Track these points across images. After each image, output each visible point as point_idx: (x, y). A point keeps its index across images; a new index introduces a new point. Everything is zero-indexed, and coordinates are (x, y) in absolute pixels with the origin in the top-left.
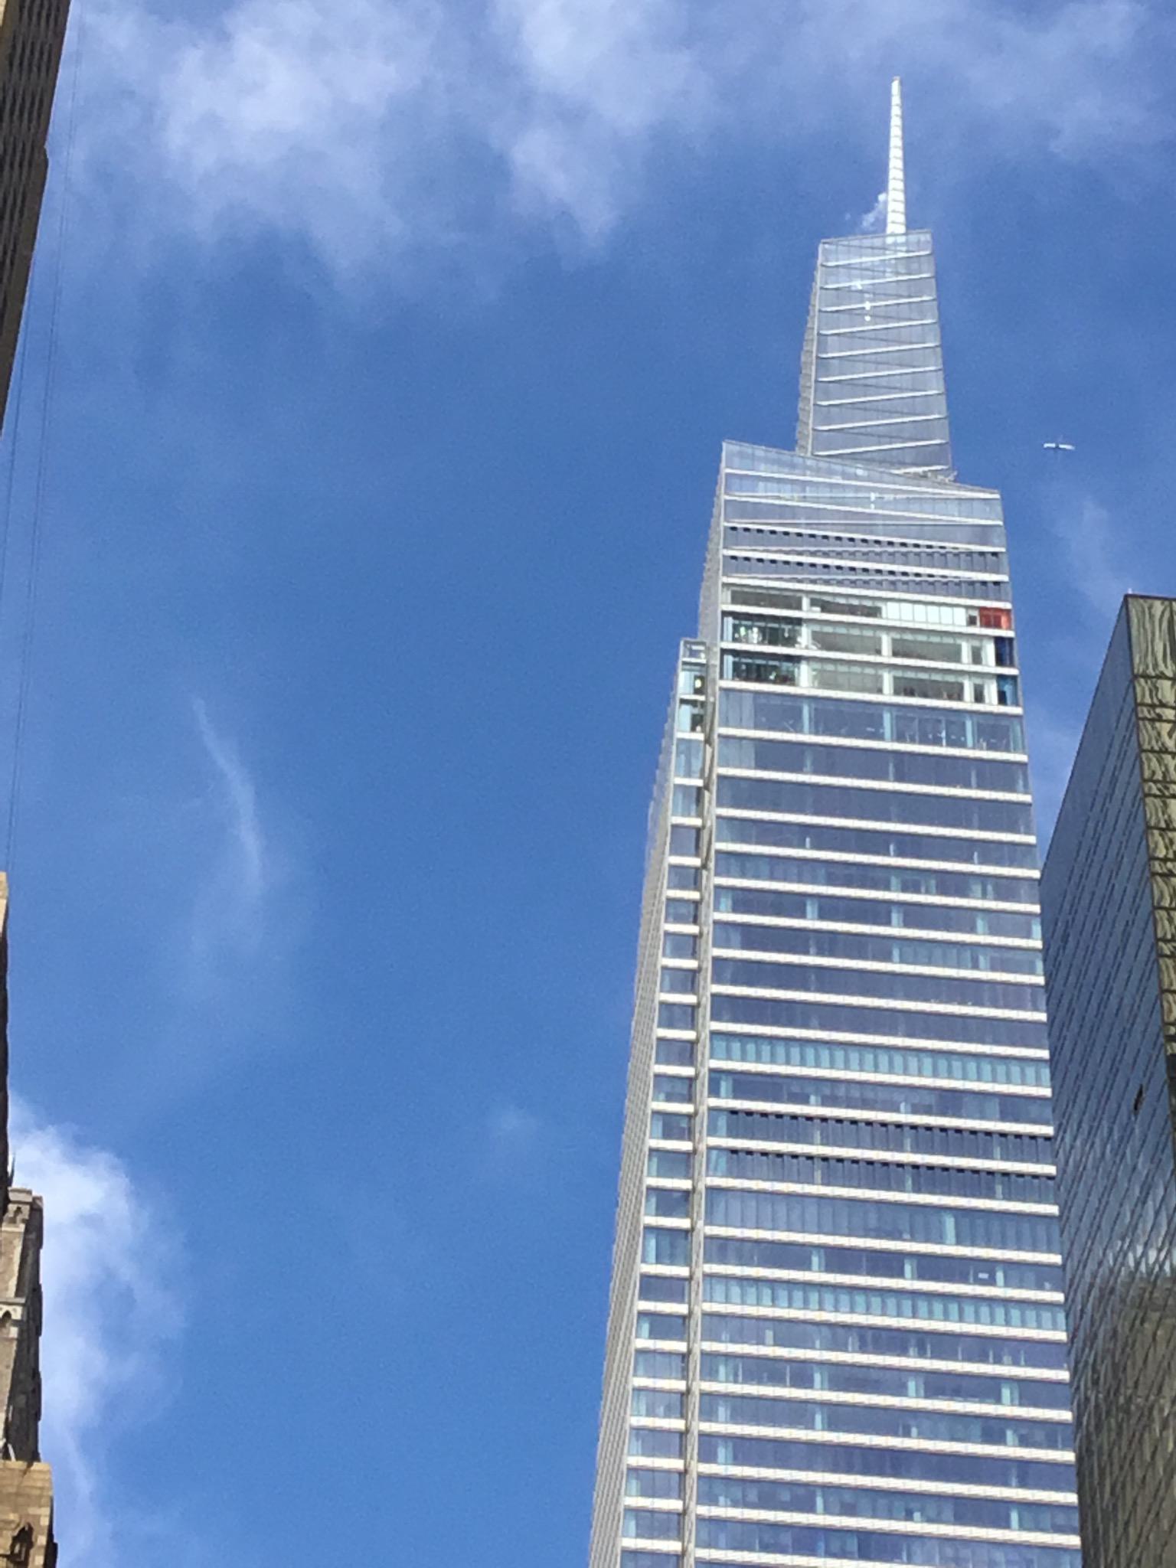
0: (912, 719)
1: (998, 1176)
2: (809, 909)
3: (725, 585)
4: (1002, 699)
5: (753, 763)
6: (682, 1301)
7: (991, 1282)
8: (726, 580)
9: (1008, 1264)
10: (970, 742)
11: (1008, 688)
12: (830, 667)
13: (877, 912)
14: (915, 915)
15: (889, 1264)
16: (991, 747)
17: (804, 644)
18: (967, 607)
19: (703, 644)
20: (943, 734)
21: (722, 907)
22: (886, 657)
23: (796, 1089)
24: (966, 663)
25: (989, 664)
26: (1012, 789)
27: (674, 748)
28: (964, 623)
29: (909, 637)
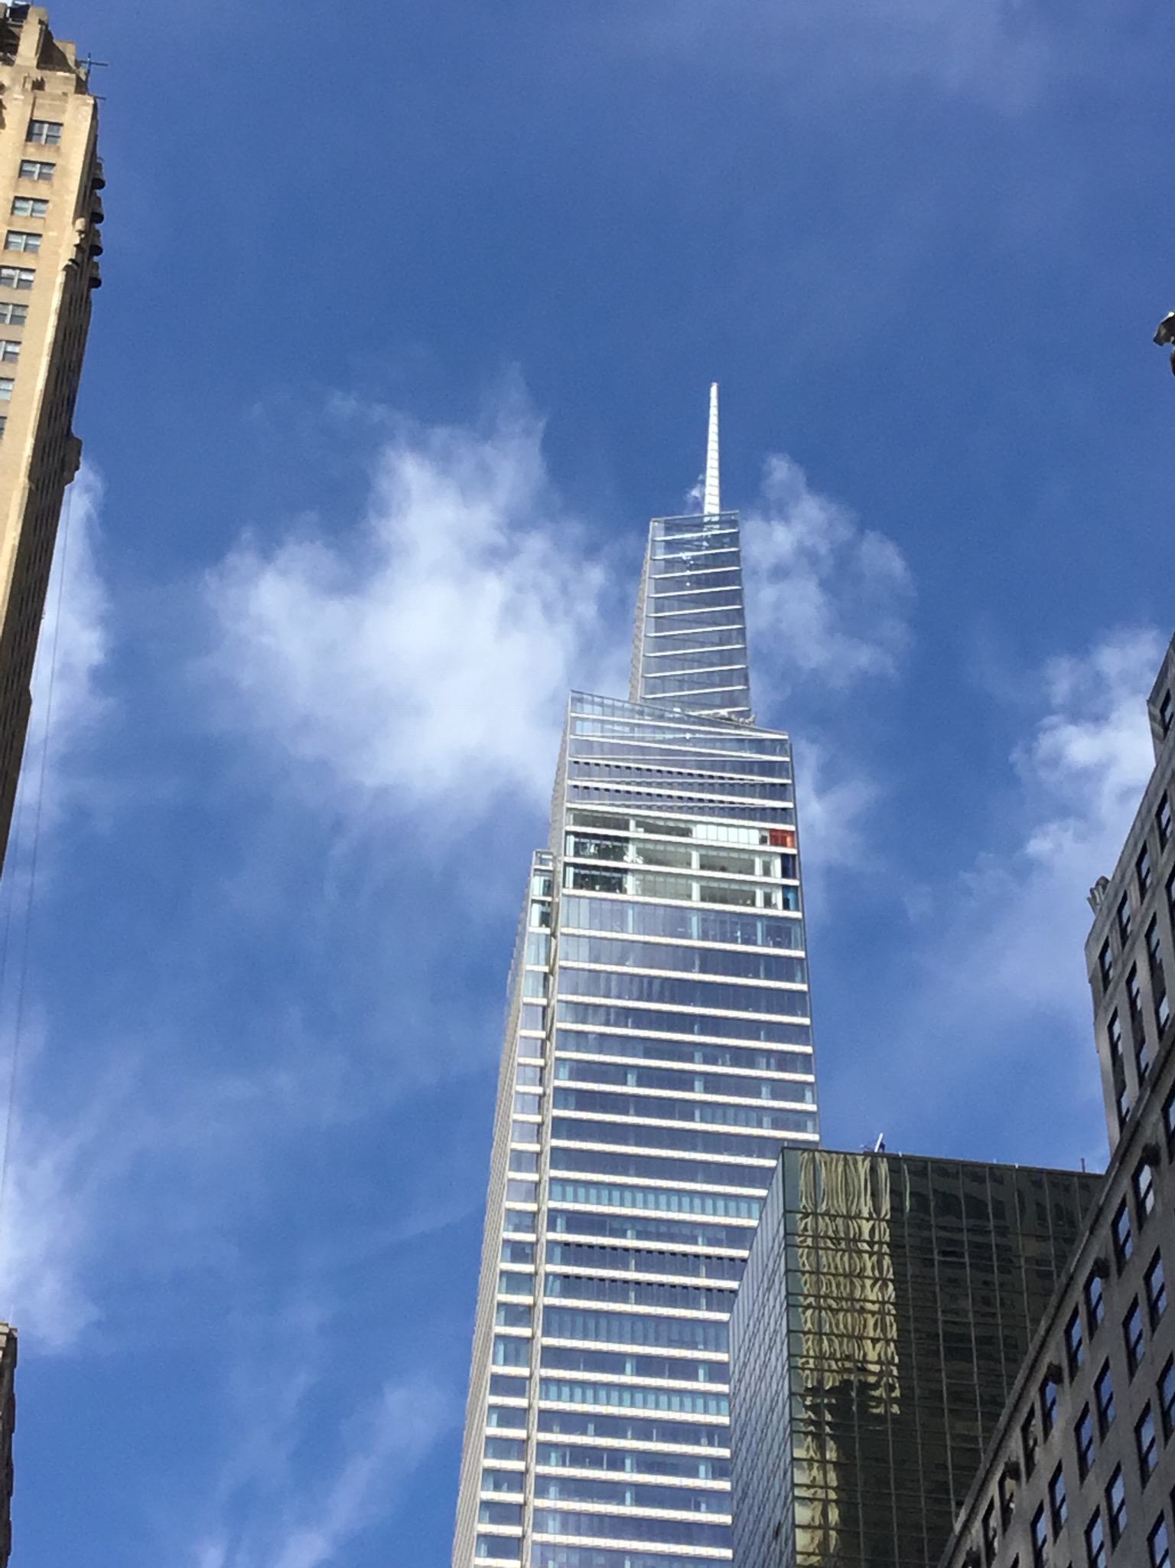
11: (791, 896)
12: (651, 878)
13: (683, 1080)
14: (714, 1083)
16: (777, 945)
18: (761, 829)
21: (561, 1075)
22: (695, 870)
24: (758, 876)
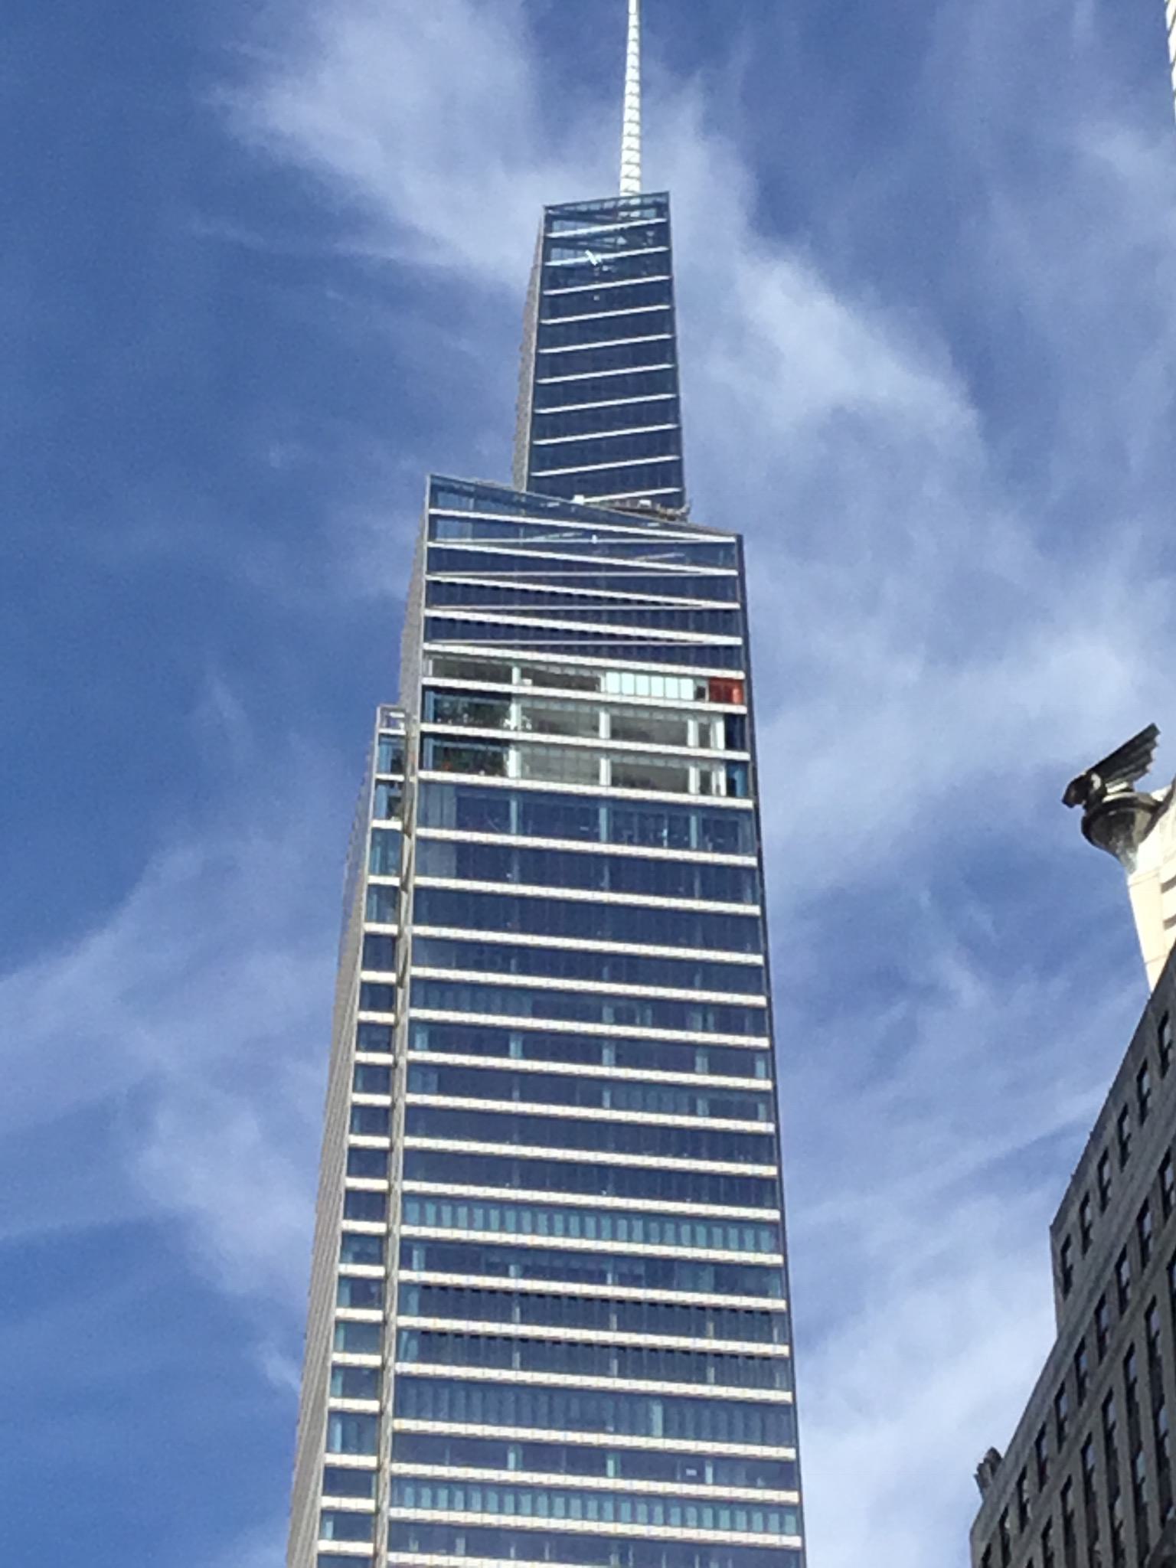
0: (631, 815)
1: (710, 1312)
2: (512, 1046)
3: (427, 653)
4: (731, 792)
5: (454, 872)
6: (368, 1496)
7: (700, 1479)
8: (427, 646)
9: (719, 1459)
10: (694, 844)
11: (738, 776)
13: (587, 1049)
14: (631, 1052)
15: (590, 1460)
16: (718, 849)
17: (513, 725)
18: (695, 677)
19: (403, 711)
20: (665, 833)
22: (603, 739)
23: (495, 1259)
24: (692, 749)
25: (718, 749)
26: (737, 899)
27: (369, 837)
28: (691, 696)
29: (629, 713)
